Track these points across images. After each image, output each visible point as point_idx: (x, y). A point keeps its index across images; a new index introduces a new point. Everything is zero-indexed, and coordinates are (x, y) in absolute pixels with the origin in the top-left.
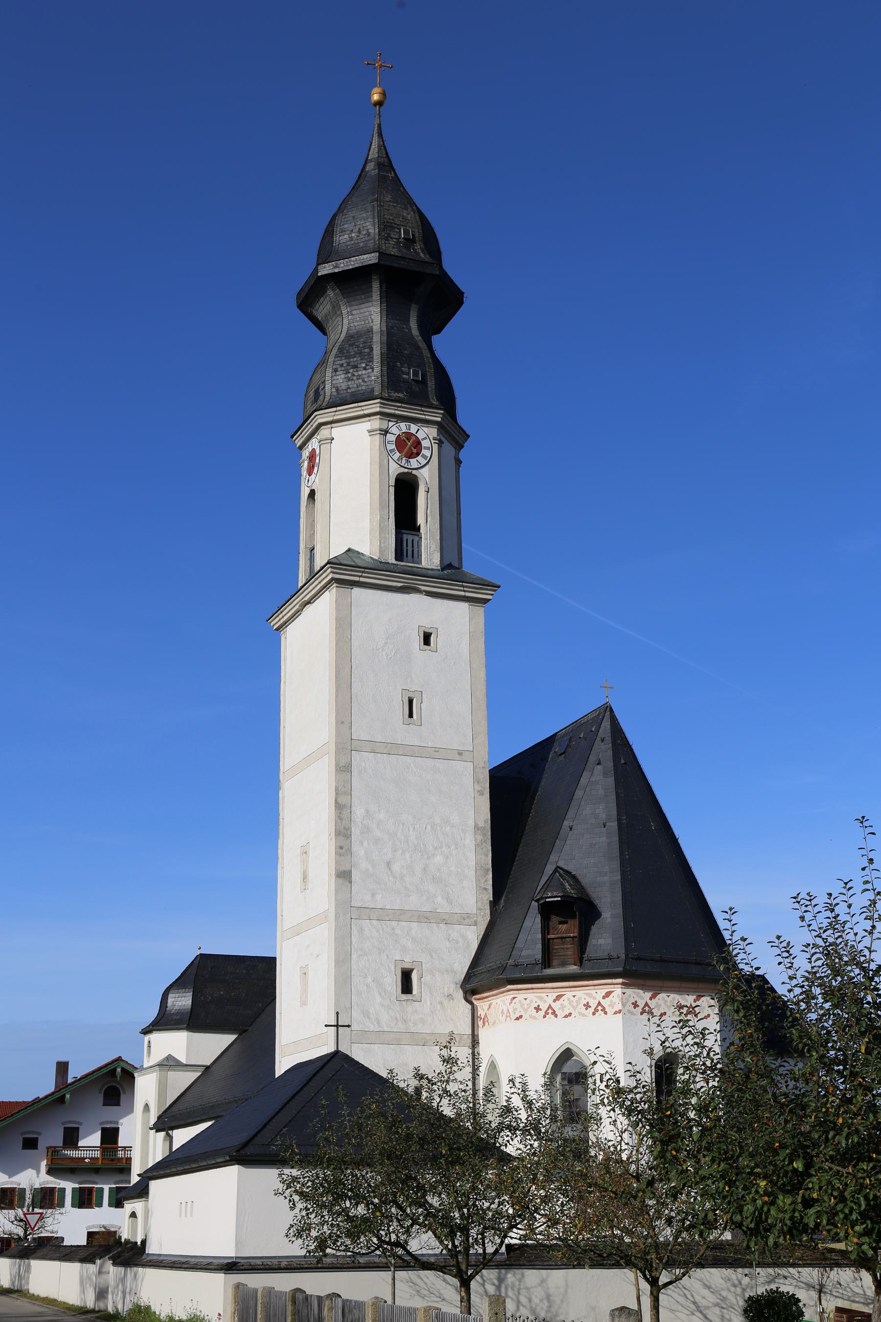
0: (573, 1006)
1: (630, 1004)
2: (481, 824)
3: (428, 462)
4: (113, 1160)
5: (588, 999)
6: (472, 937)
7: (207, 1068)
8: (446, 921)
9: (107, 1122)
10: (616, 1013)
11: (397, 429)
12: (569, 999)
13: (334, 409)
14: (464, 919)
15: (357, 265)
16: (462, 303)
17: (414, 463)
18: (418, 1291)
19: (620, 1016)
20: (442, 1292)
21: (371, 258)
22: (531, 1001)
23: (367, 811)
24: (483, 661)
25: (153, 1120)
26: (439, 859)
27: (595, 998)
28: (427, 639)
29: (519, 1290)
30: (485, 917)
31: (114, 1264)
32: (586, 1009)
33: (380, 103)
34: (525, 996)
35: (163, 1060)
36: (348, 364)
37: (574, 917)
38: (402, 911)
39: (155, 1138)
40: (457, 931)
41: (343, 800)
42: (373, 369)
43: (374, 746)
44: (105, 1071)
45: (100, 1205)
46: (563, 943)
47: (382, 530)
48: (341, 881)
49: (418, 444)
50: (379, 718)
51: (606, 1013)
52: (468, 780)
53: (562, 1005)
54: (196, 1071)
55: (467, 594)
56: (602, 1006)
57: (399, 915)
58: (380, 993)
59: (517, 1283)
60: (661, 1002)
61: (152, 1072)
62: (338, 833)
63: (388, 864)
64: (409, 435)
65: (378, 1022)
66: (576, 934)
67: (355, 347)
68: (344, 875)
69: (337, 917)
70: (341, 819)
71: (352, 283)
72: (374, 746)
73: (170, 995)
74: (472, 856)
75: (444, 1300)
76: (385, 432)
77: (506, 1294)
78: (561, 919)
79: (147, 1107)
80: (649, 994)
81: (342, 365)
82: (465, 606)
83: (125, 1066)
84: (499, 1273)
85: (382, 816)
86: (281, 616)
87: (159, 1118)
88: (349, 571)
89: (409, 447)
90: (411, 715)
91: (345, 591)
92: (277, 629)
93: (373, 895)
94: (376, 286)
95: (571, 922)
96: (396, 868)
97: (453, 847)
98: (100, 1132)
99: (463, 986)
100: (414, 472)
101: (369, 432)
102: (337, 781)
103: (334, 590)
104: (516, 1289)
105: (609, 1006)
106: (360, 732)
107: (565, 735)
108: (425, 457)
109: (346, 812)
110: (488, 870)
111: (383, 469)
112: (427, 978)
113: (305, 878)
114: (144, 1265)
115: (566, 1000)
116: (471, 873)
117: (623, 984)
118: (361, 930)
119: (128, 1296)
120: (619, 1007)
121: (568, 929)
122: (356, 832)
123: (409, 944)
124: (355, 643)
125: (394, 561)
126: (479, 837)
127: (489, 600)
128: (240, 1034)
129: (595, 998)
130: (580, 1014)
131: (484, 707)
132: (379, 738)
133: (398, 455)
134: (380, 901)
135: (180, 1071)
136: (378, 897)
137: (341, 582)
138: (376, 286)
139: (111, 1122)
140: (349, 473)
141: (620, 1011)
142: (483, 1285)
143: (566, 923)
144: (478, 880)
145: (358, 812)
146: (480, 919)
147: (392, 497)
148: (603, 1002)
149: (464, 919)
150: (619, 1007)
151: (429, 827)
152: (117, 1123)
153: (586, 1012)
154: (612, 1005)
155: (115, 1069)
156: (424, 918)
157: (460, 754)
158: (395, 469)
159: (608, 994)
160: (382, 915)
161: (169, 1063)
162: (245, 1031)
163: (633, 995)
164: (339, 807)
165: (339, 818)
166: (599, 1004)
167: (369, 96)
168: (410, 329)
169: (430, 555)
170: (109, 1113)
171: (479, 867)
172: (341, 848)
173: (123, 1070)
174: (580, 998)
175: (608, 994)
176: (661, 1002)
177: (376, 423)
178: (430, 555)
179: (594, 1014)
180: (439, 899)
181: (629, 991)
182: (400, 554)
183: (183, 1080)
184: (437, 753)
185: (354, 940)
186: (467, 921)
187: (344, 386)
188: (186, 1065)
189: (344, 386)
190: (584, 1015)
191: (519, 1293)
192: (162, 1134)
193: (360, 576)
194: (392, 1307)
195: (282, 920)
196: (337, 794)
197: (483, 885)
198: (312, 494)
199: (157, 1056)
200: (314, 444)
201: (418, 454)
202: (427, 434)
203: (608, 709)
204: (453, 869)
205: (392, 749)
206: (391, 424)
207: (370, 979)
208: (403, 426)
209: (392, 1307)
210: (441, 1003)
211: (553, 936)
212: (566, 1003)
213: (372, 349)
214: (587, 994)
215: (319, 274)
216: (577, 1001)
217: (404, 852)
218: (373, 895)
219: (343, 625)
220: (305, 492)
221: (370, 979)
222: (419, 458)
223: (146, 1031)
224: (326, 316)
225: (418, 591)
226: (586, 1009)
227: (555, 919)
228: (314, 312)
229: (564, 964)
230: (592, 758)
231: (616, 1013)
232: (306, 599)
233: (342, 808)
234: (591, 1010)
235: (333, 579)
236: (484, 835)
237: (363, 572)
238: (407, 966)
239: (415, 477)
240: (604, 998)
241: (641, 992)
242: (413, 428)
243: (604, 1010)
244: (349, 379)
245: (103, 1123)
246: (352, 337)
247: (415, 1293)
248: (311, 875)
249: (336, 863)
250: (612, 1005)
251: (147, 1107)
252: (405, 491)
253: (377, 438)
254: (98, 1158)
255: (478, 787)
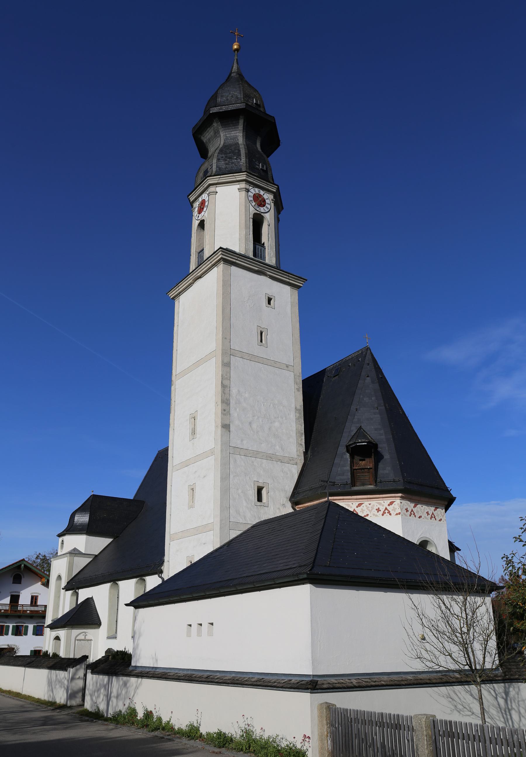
0: (369, 510)
1: (404, 509)
2: (298, 407)
3: (269, 211)
4: (16, 611)
5: (379, 506)
6: (295, 471)
7: (96, 556)
8: (281, 460)
9: (14, 592)
10: (397, 514)
11: (254, 191)
12: (366, 506)
13: (219, 176)
14: (291, 461)
15: (233, 109)
16: (279, 145)
17: (262, 209)
18: (456, 706)
19: (399, 516)
20: (471, 706)
21: (242, 106)
22: (404, 504)
23: (239, 391)
24: (298, 318)
25: (64, 584)
26: (277, 424)
27: (383, 506)
28: (269, 300)
29: (518, 701)
30: (301, 461)
31: (92, 673)
32: (378, 512)
33: (237, 50)
34: (369, 502)
35: (72, 550)
36: (226, 157)
37: (370, 457)
38: (258, 452)
39: (65, 595)
40: (287, 467)
41: (226, 382)
42: (241, 159)
43: (243, 355)
44: (16, 565)
45: (26, 634)
46: (363, 473)
47: (246, 239)
48: (224, 430)
49: (264, 201)
50: (245, 340)
51: (390, 514)
52: (291, 381)
53: (362, 509)
54: (90, 558)
55: (290, 281)
56: (388, 510)
57: (256, 454)
58: (245, 500)
59: (516, 696)
60: (419, 510)
61: (64, 557)
62: (223, 402)
63: (250, 423)
64: (260, 196)
65: (245, 517)
66: (371, 467)
67: (229, 151)
68: (226, 427)
69: (222, 451)
70: (225, 394)
71: (228, 118)
72: (243, 355)
73: (76, 515)
74: (294, 425)
75: (473, 713)
76: (248, 191)
77: (511, 706)
78: (361, 458)
79: (59, 577)
80: (413, 505)
81: (222, 157)
82: (288, 288)
83: (26, 564)
84: (505, 687)
85: (247, 395)
86: (177, 289)
87: (68, 583)
88: (228, 257)
89: (260, 201)
90: (261, 341)
91: (227, 267)
92: (173, 298)
93: (242, 441)
94: (241, 122)
95: (367, 460)
96: (254, 426)
97: (284, 418)
98: (9, 597)
99: (290, 500)
100: (262, 214)
101: (239, 189)
102: (222, 371)
103: (221, 265)
104: (516, 701)
105: (392, 510)
106: (235, 345)
107: (333, 368)
108: (268, 208)
109: (227, 391)
110: (302, 434)
111: (247, 210)
112: (271, 493)
113: (194, 432)
114: (129, 675)
115: (365, 507)
116: (294, 435)
117: (401, 497)
118: (235, 461)
119: (114, 700)
120: (399, 511)
121: (368, 463)
122: (232, 402)
123: (262, 472)
124: (233, 296)
125: (252, 257)
126: (298, 415)
127: (300, 287)
128: (114, 539)
129: (383, 506)
130: (374, 515)
131: (299, 343)
132: (245, 350)
133: (254, 204)
134: (246, 445)
135: (81, 557)
136: (245, 442)
137: (226, 261)
138: (241, 122)
139: (16, 592)
140: (226, 211)
141: (399, 513)
142: (496, 698)
143: (364, 460)
144: (297, 439)
145: (234, 391)
146: (298, 461)
147: (251, 224)
148: (388, 508)
149: (291, 461)
150: (399, 511)
151: (271, 405)
152: (19, 593)
153: (378, 514)
154: (394, 509)
155: (21, 565)
156: (270, 457)
157: (287, 367)
158: (252, 211)
159: (391, 503)
160: (247, 453)
161: (75, 553)
162: (117, 537)
163: (405, 504)
164: (224, 386)
165: (223, 392)
166: (386, 509)
167: (232, 47)
168: (257, 148)
169: (270, 258)
170: (15, 587)
171: (298, 432)
172: (225, 410)
173: (25, 565)
174: (374, 505)
175: (391, 503)
176: (419, 510)
177: (243, 185)
178: (270, 258)
179: (383, 515)
180: (277, 447)
181: (404, 502)
182: (255, 254)
183: (82, 563)
184: (275, 364)
185: (231, 466)
186: (292, 462)
187: (224, 167)
188: (85, 554)
189: (224, 167)
190: (376, 516)
191: (519, 705)
192: (70, 593)
193: (236, 260)
194: (482, 727)
195: (173, 459)
196: (222, 378)
197: (300, 442)
198: (202, 225)
199: (68, 548)
200: (205, 196)
201: (264, 206)
202: (268, 198)
203: (368, 349)
204: (284, 431)
205: (252, 358)
206: (250, 188)
207: (240, 491)
208: (256, 189)
209: (482, 727)
210: (279, 509)
211: (357, 468)
212: (365, 508)
213: (239, 151)
214: (378, 503)
215: (211, 112)
216: (371, 507)
217: (258, 417)
218: (242, 441)
219: (226, 284)
220: (195, 223)
221: (240, 491)
222: (264, 208)
223: (60, 535)
224: (209, 139)
225: (266, 275)
226: (378, 512)
227: (357, 458)
228: (202, 138)
229: (363, 484)
230: (363, 373)
231: (397, 514)
232: (199, 275)
233: (225, 387)
234: (381, 512)
235: (222, 258)
236: (300, 414)
237: (238, 257)
238: (261, 485)
239: (263, 217)
240: (389, 505)
241: (409, 502)
242: (262, 193)
243: (389, 512)
244: (227, 164)
245: (12, 592)
246: (226, 146)
247: (453, 708)
248: (198, 429)
249: (222, 419)
250: (394, 509)
251: (59, 577)
252: (257, 223)
253: (244, 193)
254: (8, 610)
255: (297, 387)
